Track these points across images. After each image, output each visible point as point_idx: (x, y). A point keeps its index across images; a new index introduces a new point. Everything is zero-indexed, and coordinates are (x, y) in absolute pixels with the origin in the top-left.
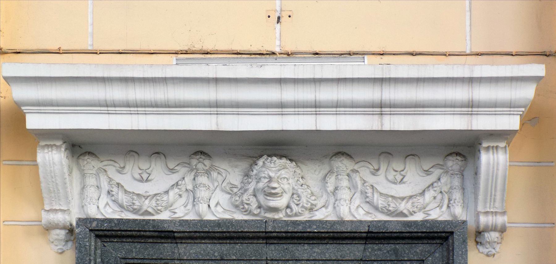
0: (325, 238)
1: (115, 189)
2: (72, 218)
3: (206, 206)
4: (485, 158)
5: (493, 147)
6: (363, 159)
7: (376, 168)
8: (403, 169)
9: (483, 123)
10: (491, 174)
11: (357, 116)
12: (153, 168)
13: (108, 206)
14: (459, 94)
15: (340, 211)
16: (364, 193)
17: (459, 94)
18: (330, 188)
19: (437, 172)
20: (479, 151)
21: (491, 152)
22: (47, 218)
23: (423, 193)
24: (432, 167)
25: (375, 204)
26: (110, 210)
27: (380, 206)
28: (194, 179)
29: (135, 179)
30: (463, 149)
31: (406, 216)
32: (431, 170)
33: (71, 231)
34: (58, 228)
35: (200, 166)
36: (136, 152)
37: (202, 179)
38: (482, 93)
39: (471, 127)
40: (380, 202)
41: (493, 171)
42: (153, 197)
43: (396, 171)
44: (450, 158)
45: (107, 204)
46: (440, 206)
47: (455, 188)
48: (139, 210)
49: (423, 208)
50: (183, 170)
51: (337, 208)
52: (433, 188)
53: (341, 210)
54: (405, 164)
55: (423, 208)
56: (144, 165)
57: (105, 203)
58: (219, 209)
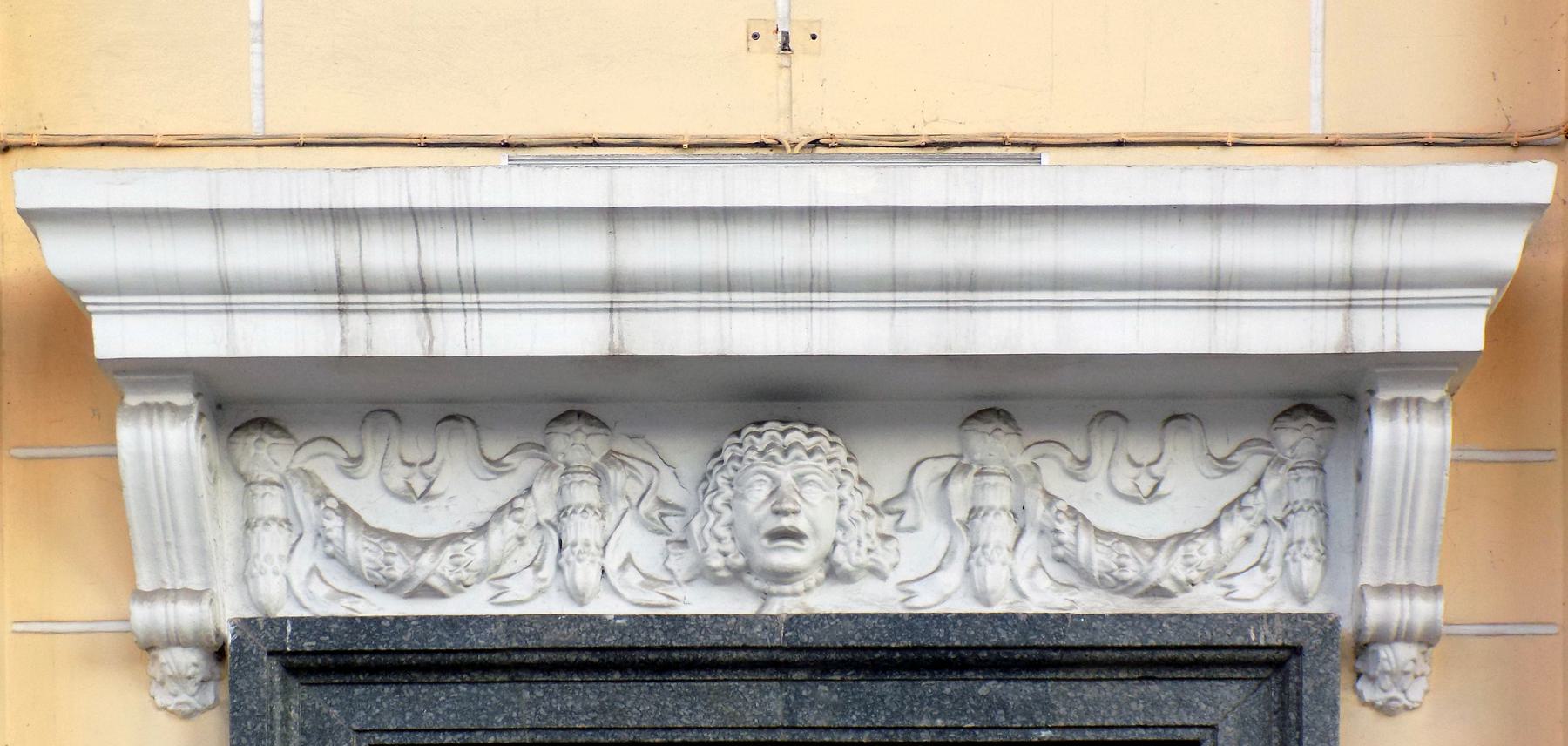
0: (408, 668)
1: (1066, 527)
2: (224, 612)
3: (595, 573)
4: (1381, 430)
5: (1408, 400)
6: (320, 434)
7: (354, 453)
8: (427, 457)
9: (1375, 332)
10: (1401, 469)
11: (1274, 313)
12: (443, 462)
13: (1040, 571)
14: (1323, 250)
15: (573, 579)
16: (321, 536)
17: (1323, 250)
18: (960, 513)
19: (1253, 463)
20: (1369, 411)
21: (1402, 412)
22: (144, 616)
23: (1213, 527)
24: (1239, 448)
25: (351, 562)
26: (321, 590)
27: (365, 565)
28: (560, 491)
29: (394, 494)
30: (1323, 402)
31: (1166, 594)
32: (1237, 458)
33: (220, 654)
34: (179, 644)
35: (577, 456)
36: (396, 416)
37: (583, 493)
38: (648, 251)
39: (369, 344)
40: (1099, 557)
41: (156, 468)
42: (1176, 545)
43: (411, 465)
44: (562, 429)
45: (314, 570)
46: (535, 565)
47: (1301, 509)
48: (1137, 584)
49: (491, 573)
50: (525, 466)
51: (976, 571)
52: (1242, 509)
53: (989, 578)
54: (1162, 442)
55: (491, 573)
56: (1143, 449)
57: (306, 569)
58: (633, 577)
